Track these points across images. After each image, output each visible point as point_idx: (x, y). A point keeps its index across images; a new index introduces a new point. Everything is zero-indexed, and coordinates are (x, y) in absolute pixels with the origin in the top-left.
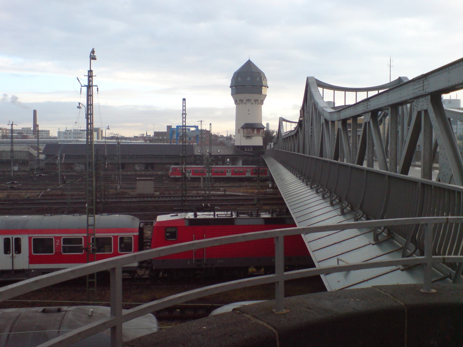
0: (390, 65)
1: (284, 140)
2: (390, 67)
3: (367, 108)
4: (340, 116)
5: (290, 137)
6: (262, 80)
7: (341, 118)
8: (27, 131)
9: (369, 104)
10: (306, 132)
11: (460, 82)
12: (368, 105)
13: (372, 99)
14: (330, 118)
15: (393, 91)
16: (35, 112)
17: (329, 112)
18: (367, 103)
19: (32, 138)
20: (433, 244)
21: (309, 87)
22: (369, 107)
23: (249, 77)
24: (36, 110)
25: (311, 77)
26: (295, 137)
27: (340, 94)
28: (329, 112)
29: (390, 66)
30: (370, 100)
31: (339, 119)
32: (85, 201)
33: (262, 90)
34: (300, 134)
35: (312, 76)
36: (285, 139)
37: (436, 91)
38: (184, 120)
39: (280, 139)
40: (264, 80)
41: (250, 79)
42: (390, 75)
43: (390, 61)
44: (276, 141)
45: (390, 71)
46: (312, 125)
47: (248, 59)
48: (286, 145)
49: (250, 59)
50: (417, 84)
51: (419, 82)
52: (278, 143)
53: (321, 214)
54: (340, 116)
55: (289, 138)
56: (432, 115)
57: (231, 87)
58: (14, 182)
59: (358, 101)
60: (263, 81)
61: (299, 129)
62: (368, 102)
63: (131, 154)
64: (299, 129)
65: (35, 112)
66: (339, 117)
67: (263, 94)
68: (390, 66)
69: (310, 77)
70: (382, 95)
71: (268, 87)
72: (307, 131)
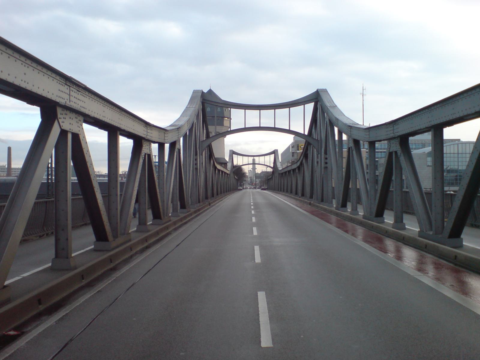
0: (363, 94)
1: (281, 175)
2: (362, 96)
5: (289, 171)
6: (223, 111)
8: (2, 169)
9: (395, 127)
10: (316, 163)
11: (477, 110)
13: (400, 121)
16: (9, 149)
19: (4, 176)
20: (6, 249)
23: (209, 108)
24: (10, 146)
25: (323, 89)
26: (297, 171)
29: (363, 95)
30: (399, 122)
33: (223, 122)
34: (305, 168)
35: (324, 88)
36: (282, 174)
37: (443, 122)
39: (276, 175)
40: (226, 111)
41: (210, 110)
42: (363, 105)
43: (363, 89)
44: (271, 177)
45: (363, 101)
46: (326, 153)
47: (210, 88)
48: (287, 180)
49: (211, 88)
52: (273, 178)
53: (157, 264)
55: (285, 174)
56: (402, 159)
60: (225, 112)
61: (304, 161)
63: (76, 193)
64: (304, 161)
65: (9, 149)
67: (224, 125)
68: (363, 95)
69: (320, 89)
72: (318, 162)
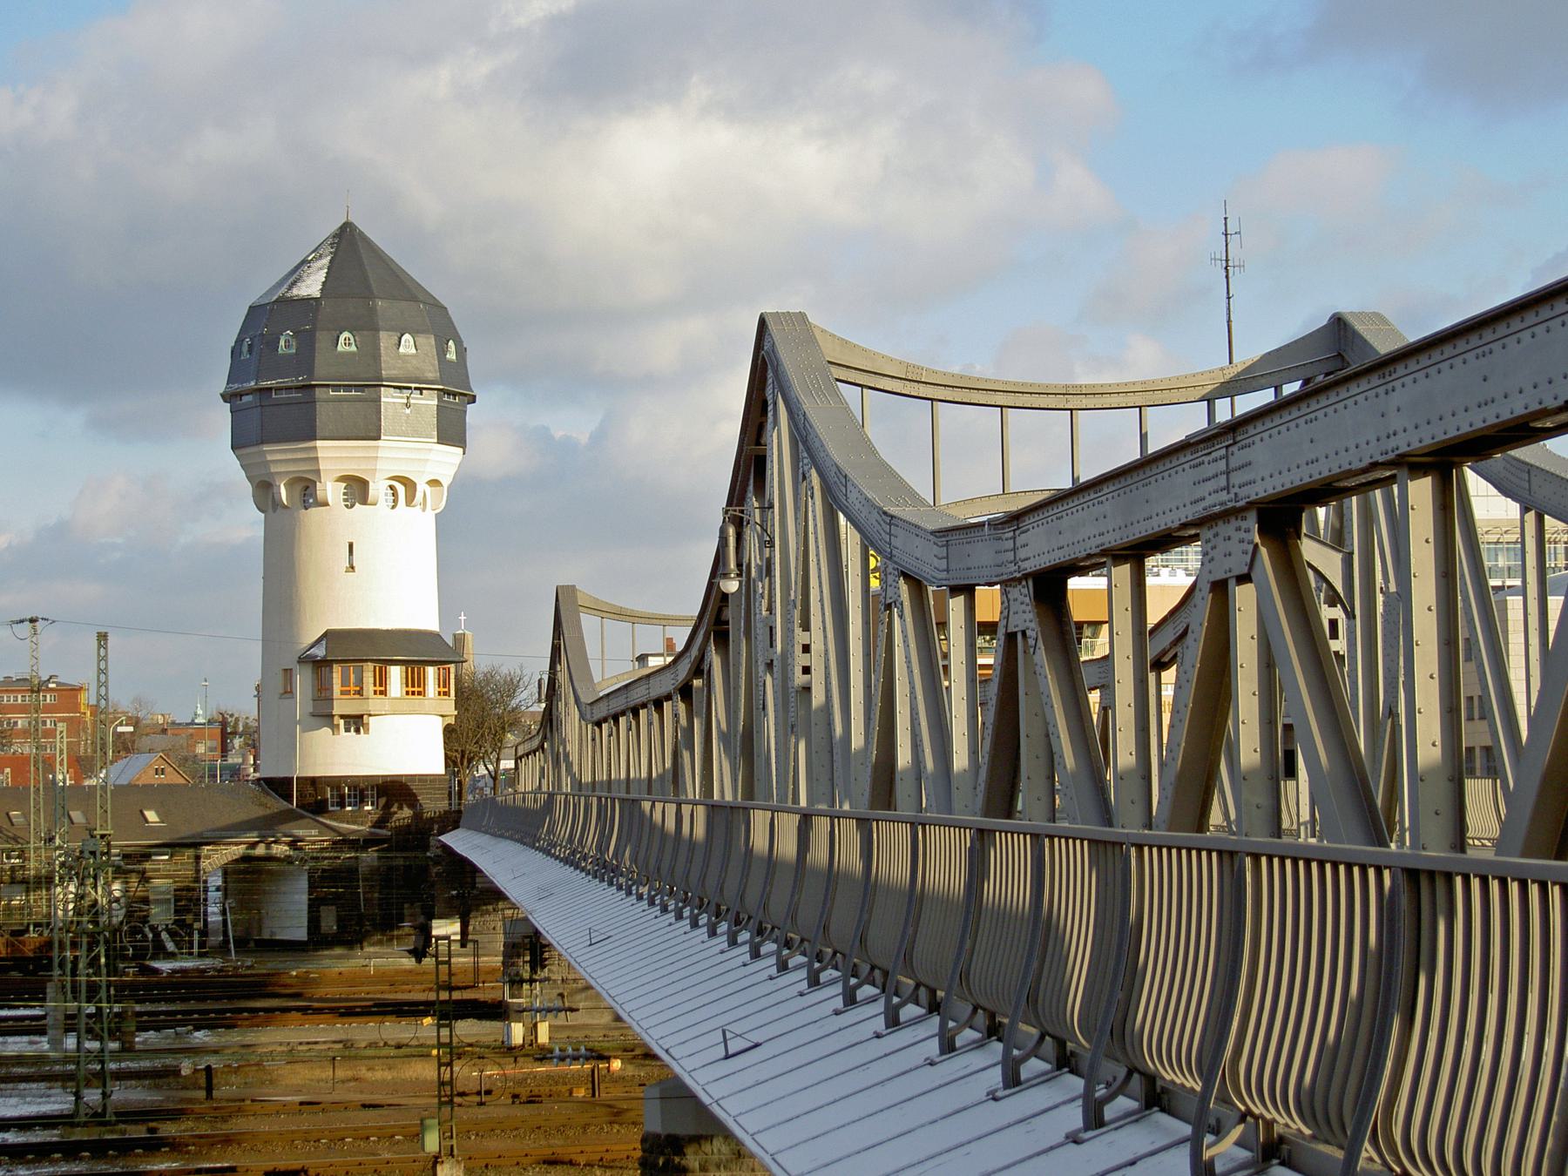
3: (1227, 488)
4: (1022, 554)
7: (1030, 566)
9: (1238, 457)
12: (1232, 465)
14: (948, 571)
15: (1460, 349)
17: (933, 533)
18: (1226, 457)
21: (776, 372)
22: (1237, 479)
27: (970, 425)
28: (931, 527)
31: (1011, 570)
32: (37, 1012)
38: (103, 678)
50: (1206, 459)
51: (1214, 455)
54: (1022, 554)
57: (226, 397)
58: (631, 1070)
59: (1152, 448)
62: (1234, 449)
66: (1011, 555)
70: (1343, 394)
71: (473, 400)
